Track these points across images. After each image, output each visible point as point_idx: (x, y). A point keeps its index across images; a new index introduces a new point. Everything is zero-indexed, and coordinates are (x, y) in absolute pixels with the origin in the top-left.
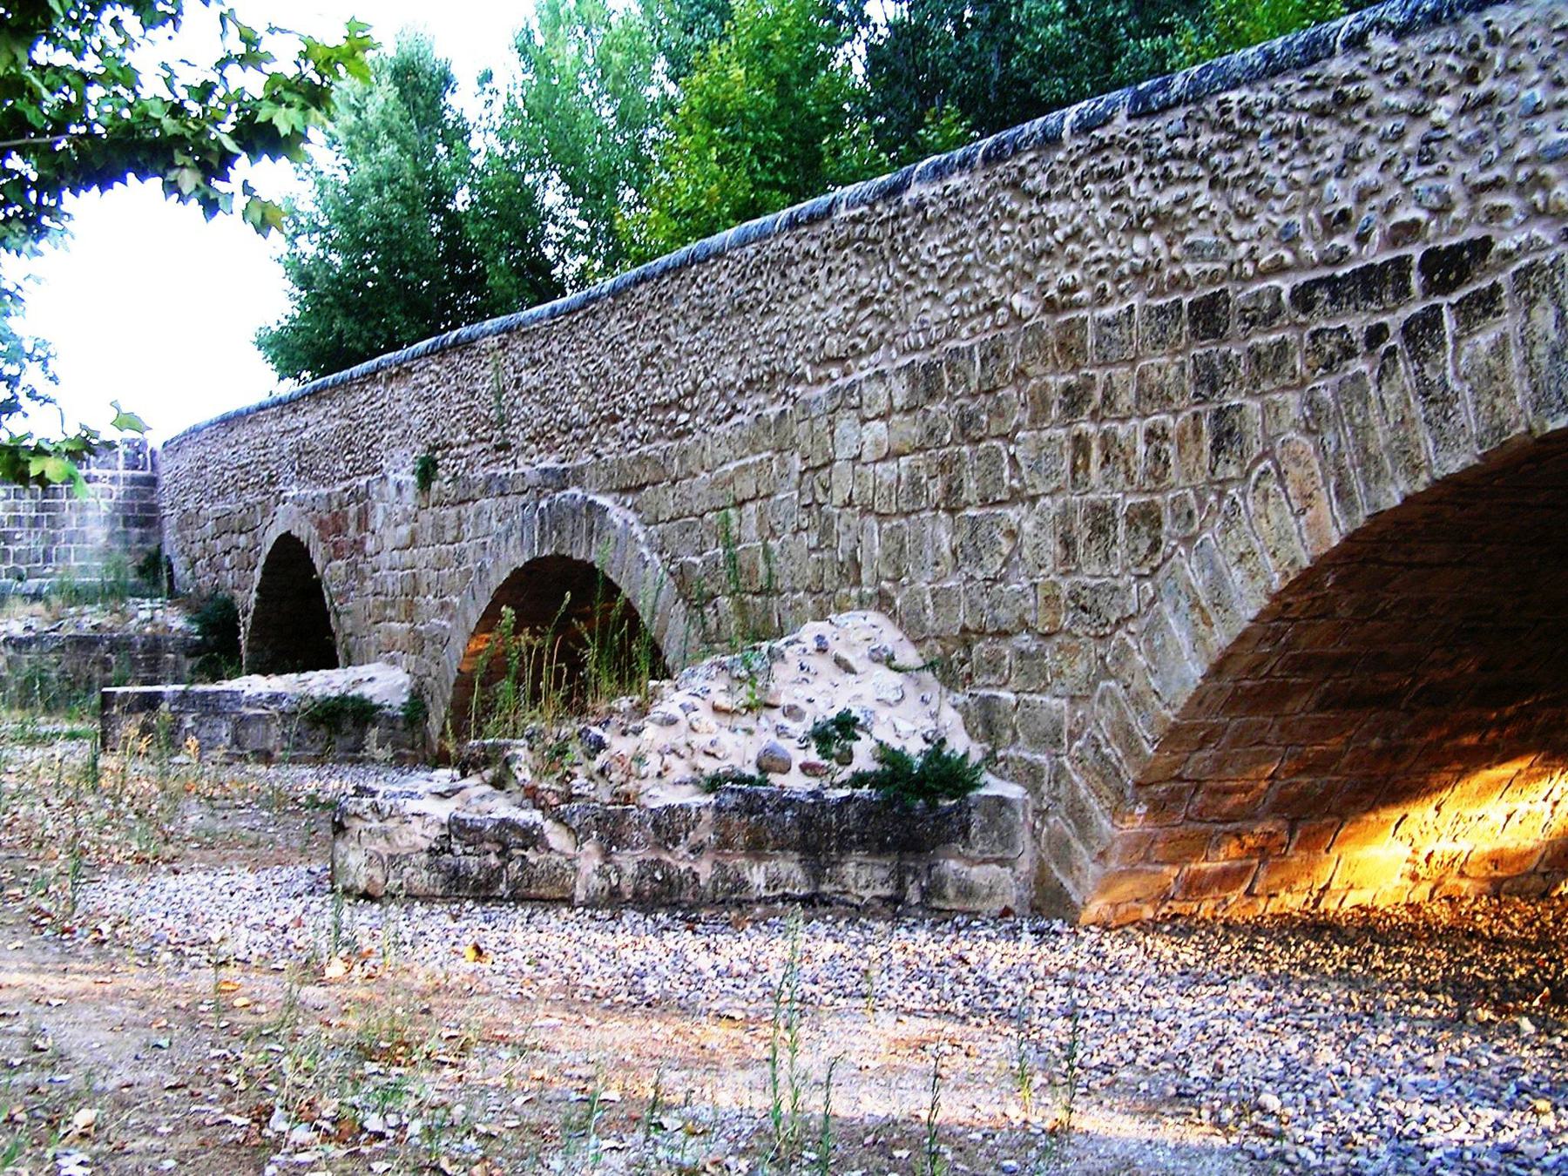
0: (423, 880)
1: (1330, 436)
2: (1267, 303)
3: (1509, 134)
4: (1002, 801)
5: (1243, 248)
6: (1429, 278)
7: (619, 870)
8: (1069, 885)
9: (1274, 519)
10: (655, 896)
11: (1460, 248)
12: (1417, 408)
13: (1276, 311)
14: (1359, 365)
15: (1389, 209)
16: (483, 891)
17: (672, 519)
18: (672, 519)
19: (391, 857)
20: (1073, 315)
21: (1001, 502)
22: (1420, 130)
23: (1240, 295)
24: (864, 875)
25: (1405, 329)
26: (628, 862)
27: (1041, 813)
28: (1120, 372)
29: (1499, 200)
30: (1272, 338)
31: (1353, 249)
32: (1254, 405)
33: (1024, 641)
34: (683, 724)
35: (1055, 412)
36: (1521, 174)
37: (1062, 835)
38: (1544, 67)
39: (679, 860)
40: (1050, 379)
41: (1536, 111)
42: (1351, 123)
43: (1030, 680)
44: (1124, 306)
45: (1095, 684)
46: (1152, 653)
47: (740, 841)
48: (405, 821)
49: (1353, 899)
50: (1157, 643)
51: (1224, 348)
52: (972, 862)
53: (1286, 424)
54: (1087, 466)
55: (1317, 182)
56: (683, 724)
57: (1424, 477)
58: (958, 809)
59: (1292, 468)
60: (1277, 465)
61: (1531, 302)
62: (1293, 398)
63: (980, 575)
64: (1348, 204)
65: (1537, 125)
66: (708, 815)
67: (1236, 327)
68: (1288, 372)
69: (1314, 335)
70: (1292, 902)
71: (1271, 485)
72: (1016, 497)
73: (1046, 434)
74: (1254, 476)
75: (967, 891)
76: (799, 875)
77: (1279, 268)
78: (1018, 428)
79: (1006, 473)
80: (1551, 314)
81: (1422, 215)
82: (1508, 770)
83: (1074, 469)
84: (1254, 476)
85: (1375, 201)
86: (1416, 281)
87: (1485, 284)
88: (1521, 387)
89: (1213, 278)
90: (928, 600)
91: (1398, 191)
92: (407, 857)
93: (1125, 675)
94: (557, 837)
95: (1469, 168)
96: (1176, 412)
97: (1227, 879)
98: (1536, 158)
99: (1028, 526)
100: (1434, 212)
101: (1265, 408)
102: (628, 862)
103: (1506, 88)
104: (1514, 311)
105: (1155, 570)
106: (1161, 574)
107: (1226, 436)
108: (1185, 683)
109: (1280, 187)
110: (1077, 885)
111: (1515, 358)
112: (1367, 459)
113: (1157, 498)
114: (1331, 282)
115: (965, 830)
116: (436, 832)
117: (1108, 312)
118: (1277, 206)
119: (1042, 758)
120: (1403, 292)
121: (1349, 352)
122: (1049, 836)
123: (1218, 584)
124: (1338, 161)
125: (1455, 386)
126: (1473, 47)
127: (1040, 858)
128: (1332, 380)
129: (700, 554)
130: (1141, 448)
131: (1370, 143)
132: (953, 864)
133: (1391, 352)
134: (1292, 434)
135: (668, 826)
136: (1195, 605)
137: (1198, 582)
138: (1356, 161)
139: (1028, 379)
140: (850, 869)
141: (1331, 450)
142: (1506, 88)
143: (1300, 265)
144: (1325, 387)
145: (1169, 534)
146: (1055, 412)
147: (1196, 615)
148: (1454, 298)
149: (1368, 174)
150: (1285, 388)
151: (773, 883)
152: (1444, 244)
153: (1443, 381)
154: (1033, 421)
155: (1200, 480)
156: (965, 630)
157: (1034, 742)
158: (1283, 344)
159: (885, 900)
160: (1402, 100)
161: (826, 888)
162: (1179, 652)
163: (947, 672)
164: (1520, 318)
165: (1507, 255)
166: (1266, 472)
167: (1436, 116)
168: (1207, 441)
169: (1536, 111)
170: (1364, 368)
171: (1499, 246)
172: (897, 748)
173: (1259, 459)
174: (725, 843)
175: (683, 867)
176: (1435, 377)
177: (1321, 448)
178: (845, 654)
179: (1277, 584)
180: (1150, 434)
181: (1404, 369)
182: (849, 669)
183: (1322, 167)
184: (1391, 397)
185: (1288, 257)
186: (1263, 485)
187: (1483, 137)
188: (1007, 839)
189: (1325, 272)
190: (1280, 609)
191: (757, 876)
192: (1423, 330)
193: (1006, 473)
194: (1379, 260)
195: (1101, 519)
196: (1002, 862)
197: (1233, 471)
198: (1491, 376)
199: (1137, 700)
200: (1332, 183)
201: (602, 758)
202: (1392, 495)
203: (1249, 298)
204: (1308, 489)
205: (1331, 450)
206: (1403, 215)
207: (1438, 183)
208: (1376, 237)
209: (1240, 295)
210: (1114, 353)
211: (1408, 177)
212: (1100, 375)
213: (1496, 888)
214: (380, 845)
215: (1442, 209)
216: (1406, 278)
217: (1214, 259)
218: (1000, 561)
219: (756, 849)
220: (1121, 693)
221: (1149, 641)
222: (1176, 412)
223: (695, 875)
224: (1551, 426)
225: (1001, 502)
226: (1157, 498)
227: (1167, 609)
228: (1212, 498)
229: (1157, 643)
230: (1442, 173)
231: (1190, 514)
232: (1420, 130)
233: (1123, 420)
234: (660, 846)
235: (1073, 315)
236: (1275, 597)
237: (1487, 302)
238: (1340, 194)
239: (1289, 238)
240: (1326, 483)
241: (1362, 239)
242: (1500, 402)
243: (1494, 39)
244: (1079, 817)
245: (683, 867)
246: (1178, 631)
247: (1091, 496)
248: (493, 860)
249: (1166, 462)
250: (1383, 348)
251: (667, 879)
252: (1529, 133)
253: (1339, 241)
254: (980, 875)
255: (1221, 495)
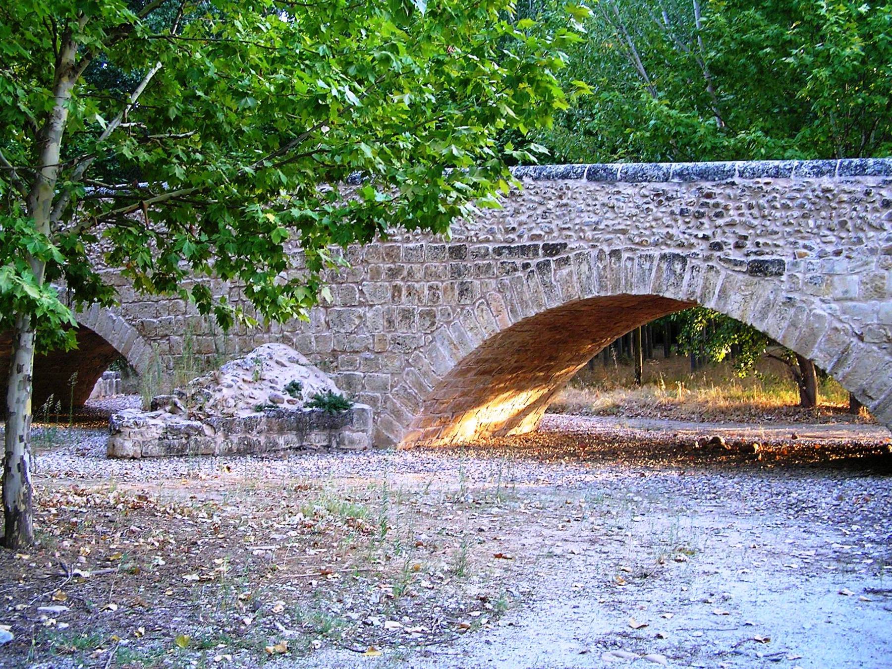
0: (155, 450)
1: (508, 293)
2: (483, 251)
3: (573, 216)
4: (363, 410)
5: (473, 233)
6: (546, 251)
7: (232, 442)
8: (392, 437)
9: (486, 317)
10: (245, 450)
11: (557, 245)
12: (541, 288)
13: (487, 254)
14: (519, 274)
15: (531, 229)
16: (180, 453)
17: (134, 302)
18: (134, 302)
19: (143, 442)
20: (394, 244)
21: (354, 306)
22: (543, 208)
23: (472, 247)
24: (318, 437)
25: (538, 265)
26: (235, 438)
27: (378, 414)
28: (416, 267)
29: (569, 233)
30: (485, 262)
31: (517, 239)
32: (477, 283)
33: (367, 354)
34: (235, 387)
35: (383, 276)
36: (577, 227)
37: (388, 421)
38: (584, 200)
39: (253, 436)
40: (381, 265)
41: (582, 211)
42: (516, 201)
43: (371, 368)
44: (419, 245)
45: (404, 369)
46: (431, 358)
47: (275, 428)
48: (149, 427)
49: (462, 439)
50: (434, 355)
51: (465, 263)
52: (353, 431)
53: (490, 289)
54: (400, 296)
55: (503, 217)
56: (235, 387)
57: (543, 308)
58: (349, 413)
59: (493, 303)
60: (487, 301)
61: (581, 263)
62: (493, 282)
63: (343, 331)
64: (515, 226)
65: (582, 215)
66: (264, 420)
67: (469, 257)
68: (491, 272)
69: (502, 263)
70: (447, 440)
71: (485, 307)
72: (361, 304)
73: (378, 284)
74: (477, 304)
75: (352, 442)
76: (296, 440)
77: (487, 241)
78: (363, 280)
79: (357, 296)
80: (587, 267)
81: (543, 233)
82: (506, 395)
83: (393, 296)
84: (477, 304)
85: (525, 226)
86: (541, 252)
87: (565, 256)
88: (577, 286)
89: (459, 240)
90: (313, 339)
91: (534, 225)
92: (150, 442)
93: (420, 366)
94: (208, 431)
95: (560, 223)
96: (442, 282)
97: (435, 432)
98: (582, 224)
99: (369, 315)
100: (546, 233)
101: (482, 284)
102: (235, 438)
103: (572, 202)
104: (575, 264)
105: (432, 332)
106: (435, 334)
107: (464, 291)
108: (447, 368)
109: (488, 216)
110: (396, 436)
111: (575, 278)
112: (522, 302)
113: (434, 309)
114: (509, 248)
115: (352, 420)
116: (161, 431)
117: (411, 245)
118: (487, 222)
119: (379, 395)
120: (536, 254)
121: (515, 270)
122: (381, 421)
123: (462, 336)
124: (512, 212)
125: (555, 283)
126: (561, 189)
127: (377, 429)
128: (509, 277)
129: (157, 317)
130: (426, 292)
131: (523, 209)
132: (347, 433)
133: (532, 271)
134: (493, 292)
135: (249, 425)
136: (452, 343)
137: (453, 336)
138: (518, 213)
139: (369, 264)
140: (313, 436)
141: (508, 298)
142: (572, 202)
143: (495, 241)
144: (507, 280)
145: (439, 320)
146: (383, 276)
147: (452, 346)
148: (555, 258)
149: (523, 218)
150: (489, 278)
151: (287, 443)
152: (551, 243)
153: (551, 281)
154: (372, 278)
155: (454, 304)
156: (334, 350)
157: (373, 389)
158: (489, 265)
159: (324, 447)
160: (536, 199)
161: (304, 444)
162: (444, 357)
163: (325, 367)
164: (577, 267)
165: (572, 249)
166: (482, 303)
167: (549, 206)
168: (457, 292)
169: (582, 211)
170: (522, 275)
171: (570, 246)
172: (338, 395)
173: (479, 299)
174: (270, 429)
175: (255, 439)
176: (548, 280)
177: (504, 297)
178: (279, 360)
179: (487, 337)
180: (431, 288)
181: (537, 277)
182: (283, 365)
183: (506, 213)
184: (532, 285)
185: (491, 238)
186: (481, 307)
187: (564, 215)
188: (365, 423)
189: (507, 245)
190: (486, 345)
191: (281, 441)
192: (543, 267)
193: (357, 296)
194: (527, 244)
195: (407, 315)
196: (363, 431)
197: (468, 302)
198: (567, 282)
199: (425, 374)
200: (509, 218)
201: (212, 401)
202: (532, 312)
203: (475, 249)
204: (500, 309)
205: (508, 298)
206: (534, 232)
207: (549, 225)
208: (526, 236)
209: (472, 247)
210: (414, 259)
211: (538, 221)
212: (407, 266)
213: (494, 435)
214: (139, 438)
215: (551, 231)
216: (537, 251)
217: (460, 234)
218: (354, 326)
219: (281, 431)
220: (417, 371)
221: (430, 355)
222: (442, 282)
223: (259, 442)
224: (586, 297)
225: (354, 306)
226: (434, 309)
227: (438, 344)
228: (459, 310)
229: (434, 355)
230: (550, 222)
231: (449, 314)
232: (543, 208)
233: (417, 282)
234: (247, 432)
235: (394, 244)
236: (485, 342)
237: (566, 261)
238: (512, 222)
239: (491, 231)
240: (506, 308)
241: (520, 237)
242: (570, 289)
243: (568, 188)
244: (398, 414)
245: (255, 439)
246: (444, 351)
247: (402, 306)
248: (184, 441)
249: (438, 297)
250: (529, 270)
251: (249, 444)
252: (579, 217)
253: (511, 236)
254: (356, 436)
255: (462, 309)
